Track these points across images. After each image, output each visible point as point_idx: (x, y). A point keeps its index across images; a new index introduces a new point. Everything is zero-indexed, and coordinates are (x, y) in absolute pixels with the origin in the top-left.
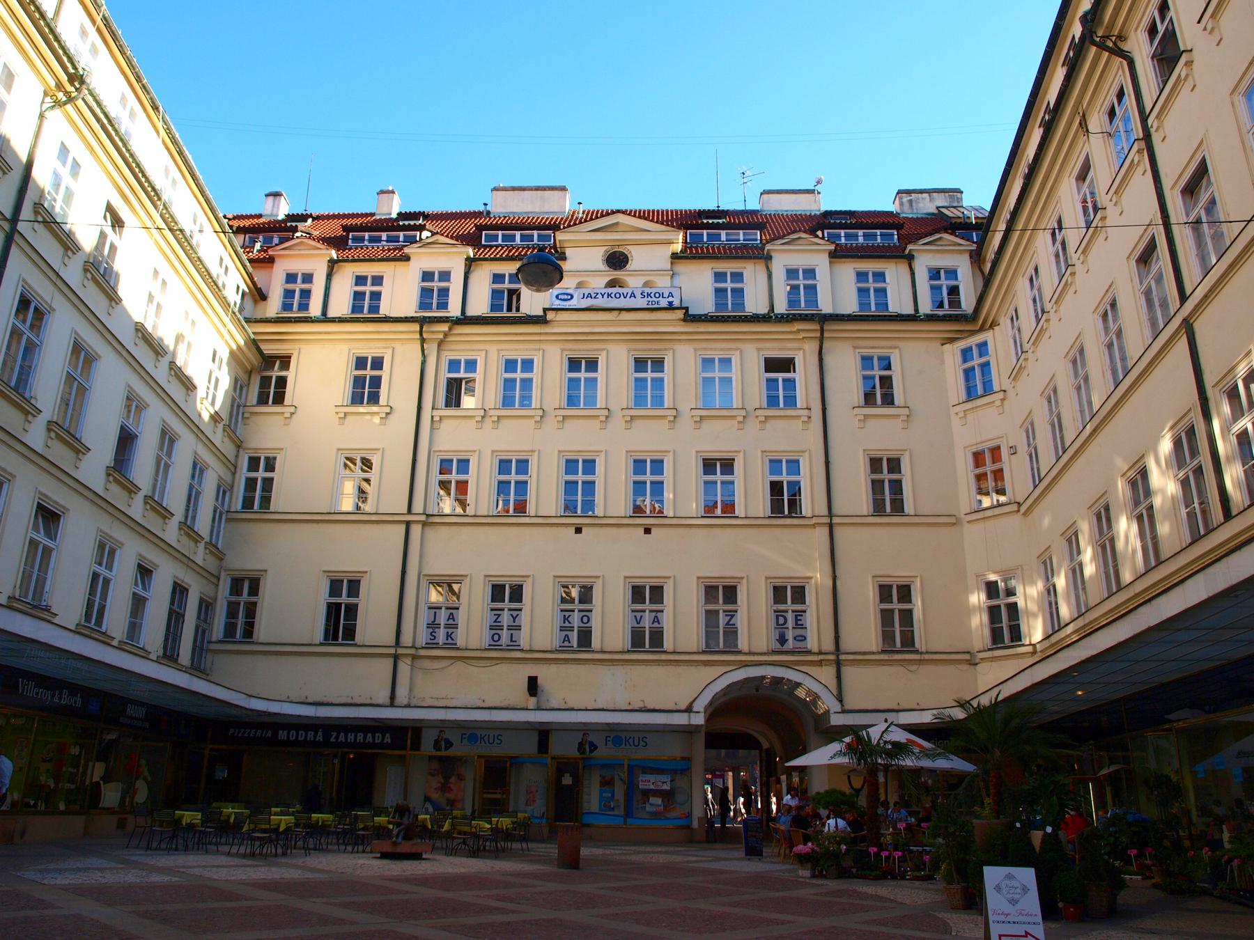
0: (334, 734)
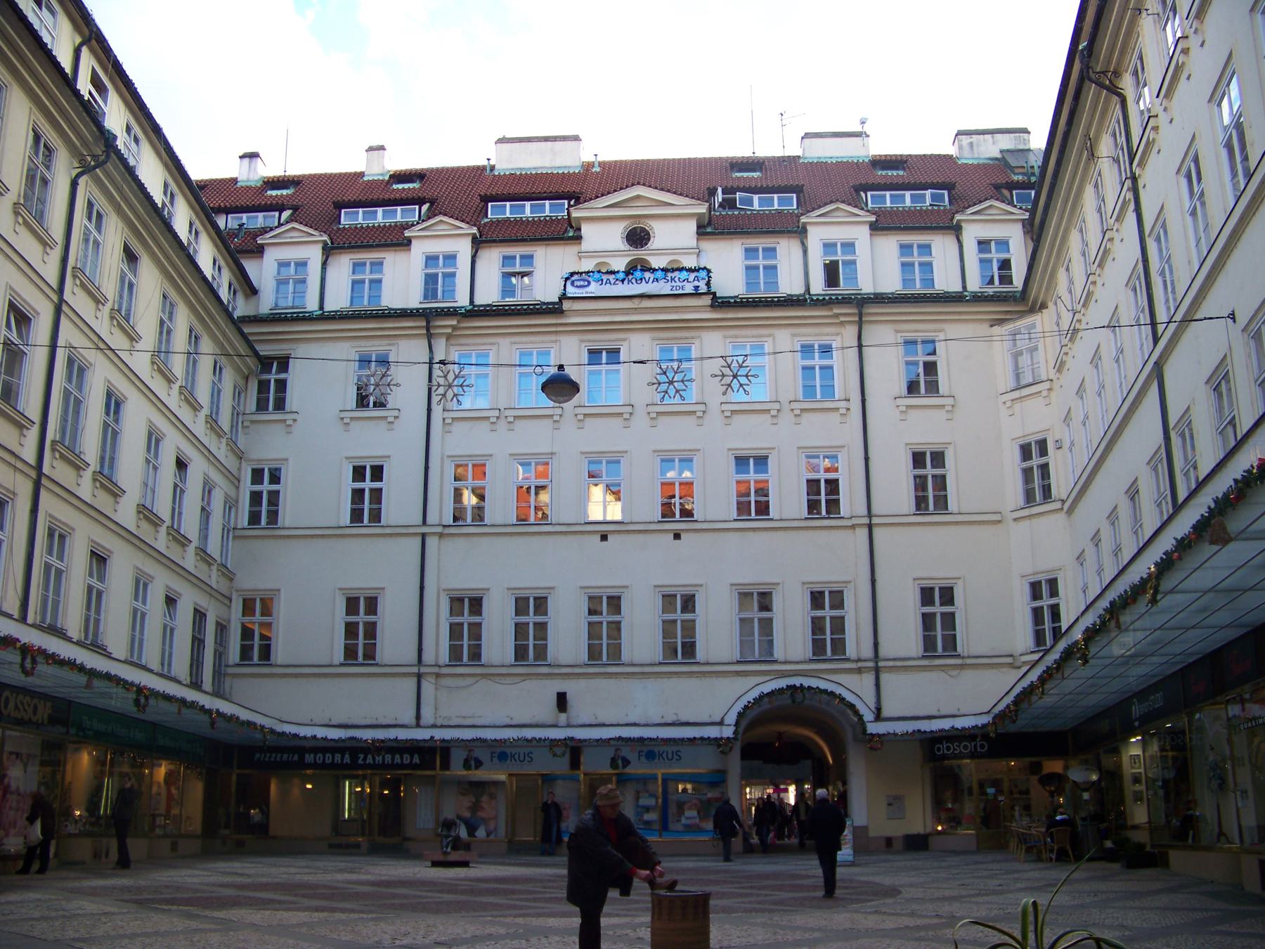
0: (362, 756)
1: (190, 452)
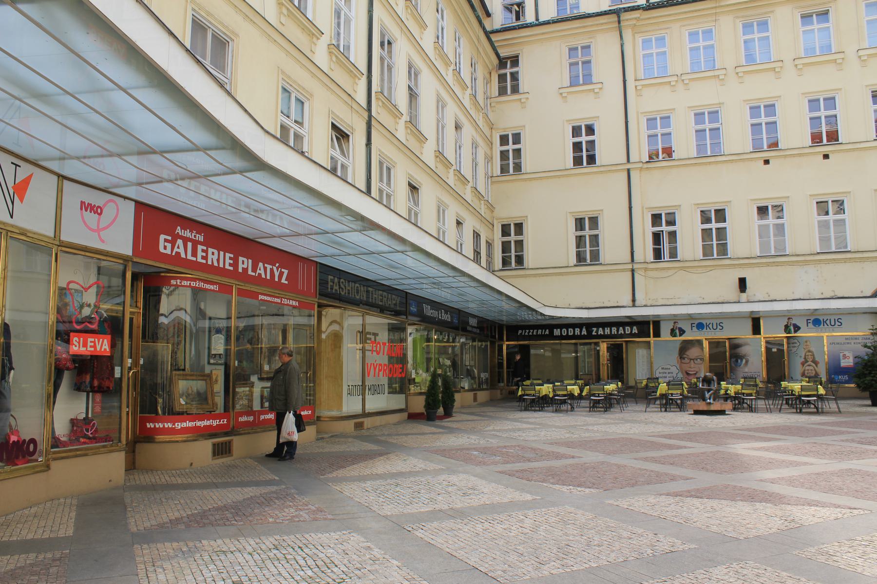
1: (463, 120)
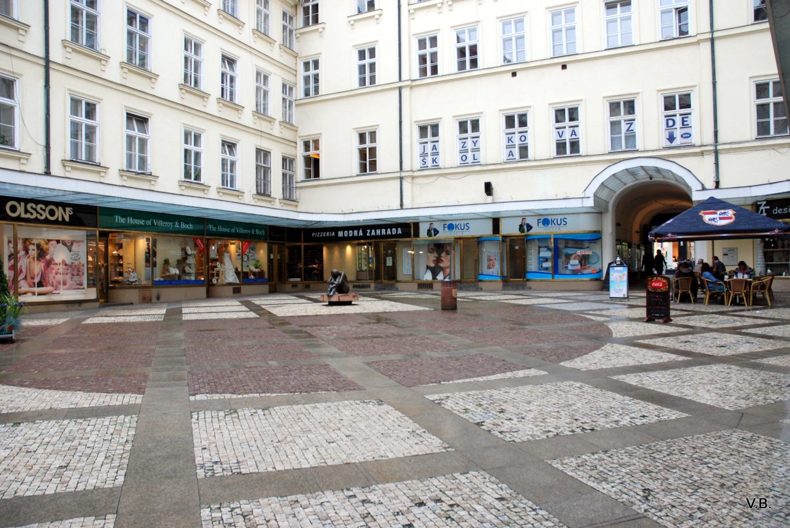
0: (369, 231)
